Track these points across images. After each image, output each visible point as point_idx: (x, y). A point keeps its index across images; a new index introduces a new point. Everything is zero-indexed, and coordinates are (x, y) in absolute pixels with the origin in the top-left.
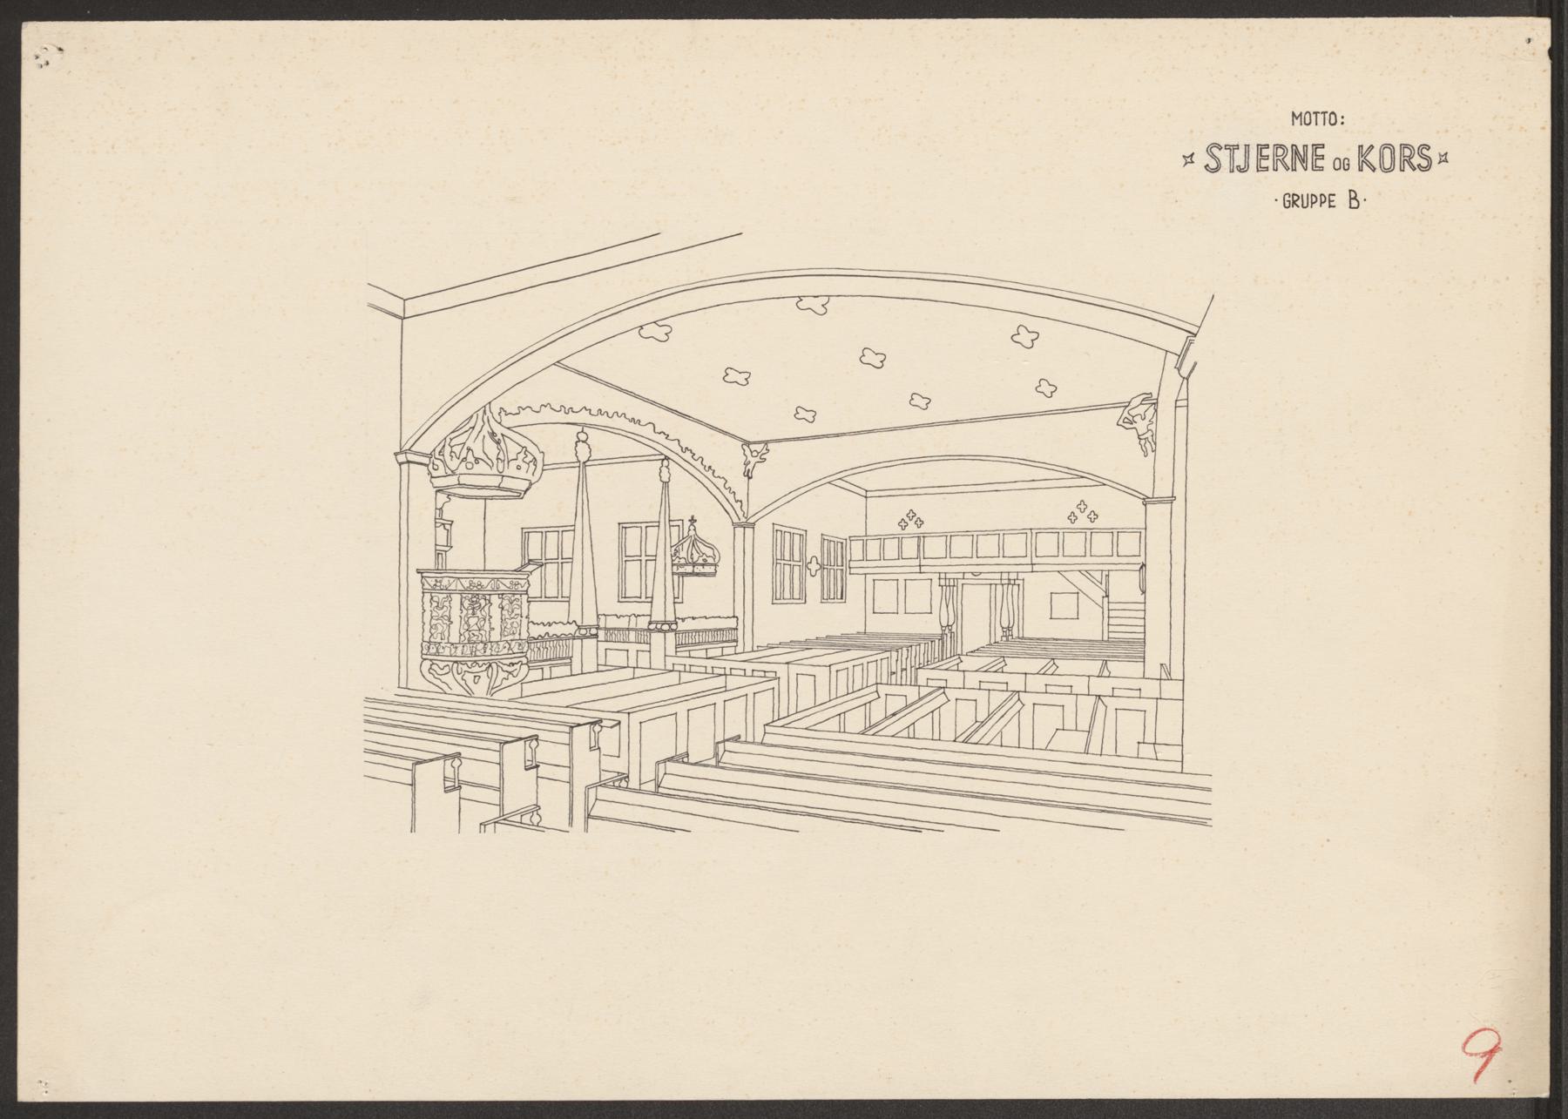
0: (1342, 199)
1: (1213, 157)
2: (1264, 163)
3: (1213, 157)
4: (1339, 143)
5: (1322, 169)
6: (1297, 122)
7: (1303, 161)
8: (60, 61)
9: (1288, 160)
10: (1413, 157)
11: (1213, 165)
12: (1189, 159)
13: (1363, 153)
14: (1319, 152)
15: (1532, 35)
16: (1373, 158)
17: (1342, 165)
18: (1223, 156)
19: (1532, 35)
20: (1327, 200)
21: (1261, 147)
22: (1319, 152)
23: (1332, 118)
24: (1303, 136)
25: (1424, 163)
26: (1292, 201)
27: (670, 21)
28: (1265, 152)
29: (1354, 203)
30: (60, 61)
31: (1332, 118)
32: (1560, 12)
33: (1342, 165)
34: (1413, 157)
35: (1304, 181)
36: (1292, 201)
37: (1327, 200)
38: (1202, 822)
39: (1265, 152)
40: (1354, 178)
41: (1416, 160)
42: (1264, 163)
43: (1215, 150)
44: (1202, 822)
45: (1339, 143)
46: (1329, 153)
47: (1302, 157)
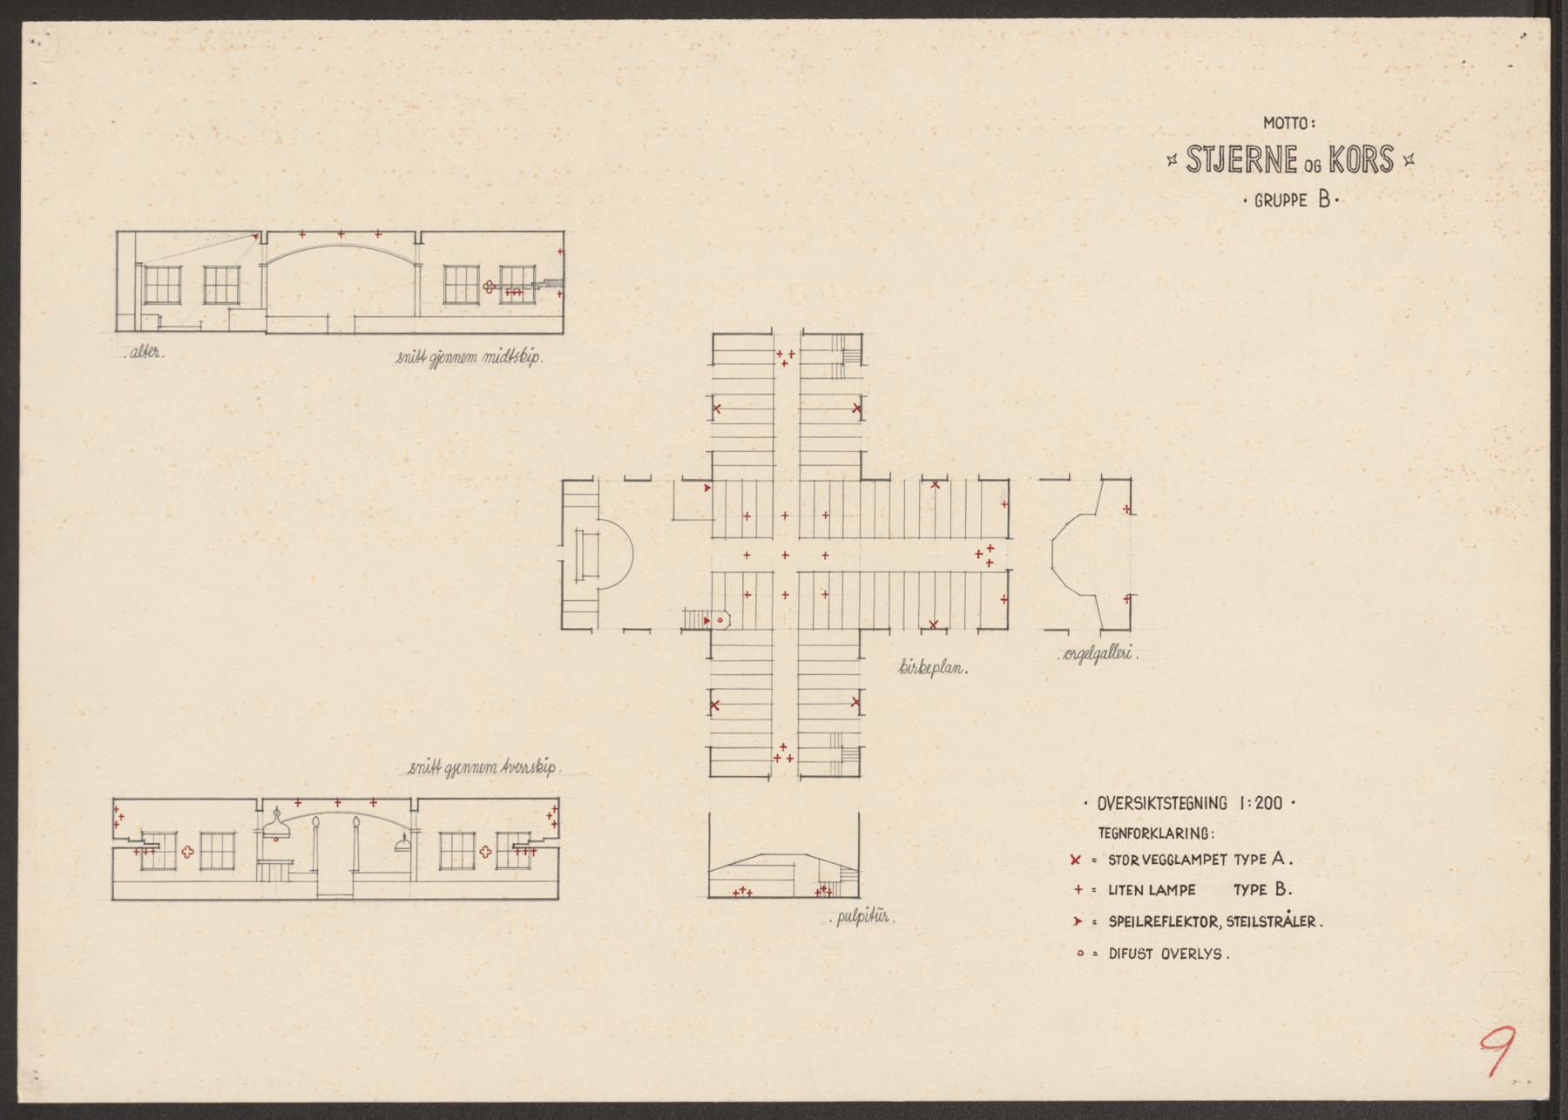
0: (1312, 199)
1: (1195, 158)
2: (1237, 165)
3: (1195, 158)
4: (1311, 145)
5: (1295, 170)
6: (1269, 126)
7: (1269, 157)
8: (59, 59)
9: (1262, 162)
10: (1368, 159)
11: (1194, 165)
12: (1172, 160)
13: (1334, 153)
14: (1293, 153)
15: (1532, 37)
16: (1342, 159)
17: (1314, 166)
18: (1202, 155)
19: (1532, 37)
20: (1297, 199)
21: (1233, 148)
22: (1293, 153)
23: (1301, 122)
24: (1273, 138)
25: (1195, 152)
26: (1266, 200)
27: (735, 21)
28: (1237, 153)
29: (1325, 202)
30: (59, 59)
31: (1301, 122)
32: (1559, 13)
33: (1314, 166)
34: (1368, 159)
35: (1278, 183)
36: (1266, 200)
37: (1297, 199)
38: (1106, 803)
39: (1237, 153)
40: (1327, 179)
41: (1380, 161)
42: (1237, 165)
43: (1195, 152)
44: (1106, 803)
45: (1311, 145)
46: (1301, 156)
47: (1281, 160)
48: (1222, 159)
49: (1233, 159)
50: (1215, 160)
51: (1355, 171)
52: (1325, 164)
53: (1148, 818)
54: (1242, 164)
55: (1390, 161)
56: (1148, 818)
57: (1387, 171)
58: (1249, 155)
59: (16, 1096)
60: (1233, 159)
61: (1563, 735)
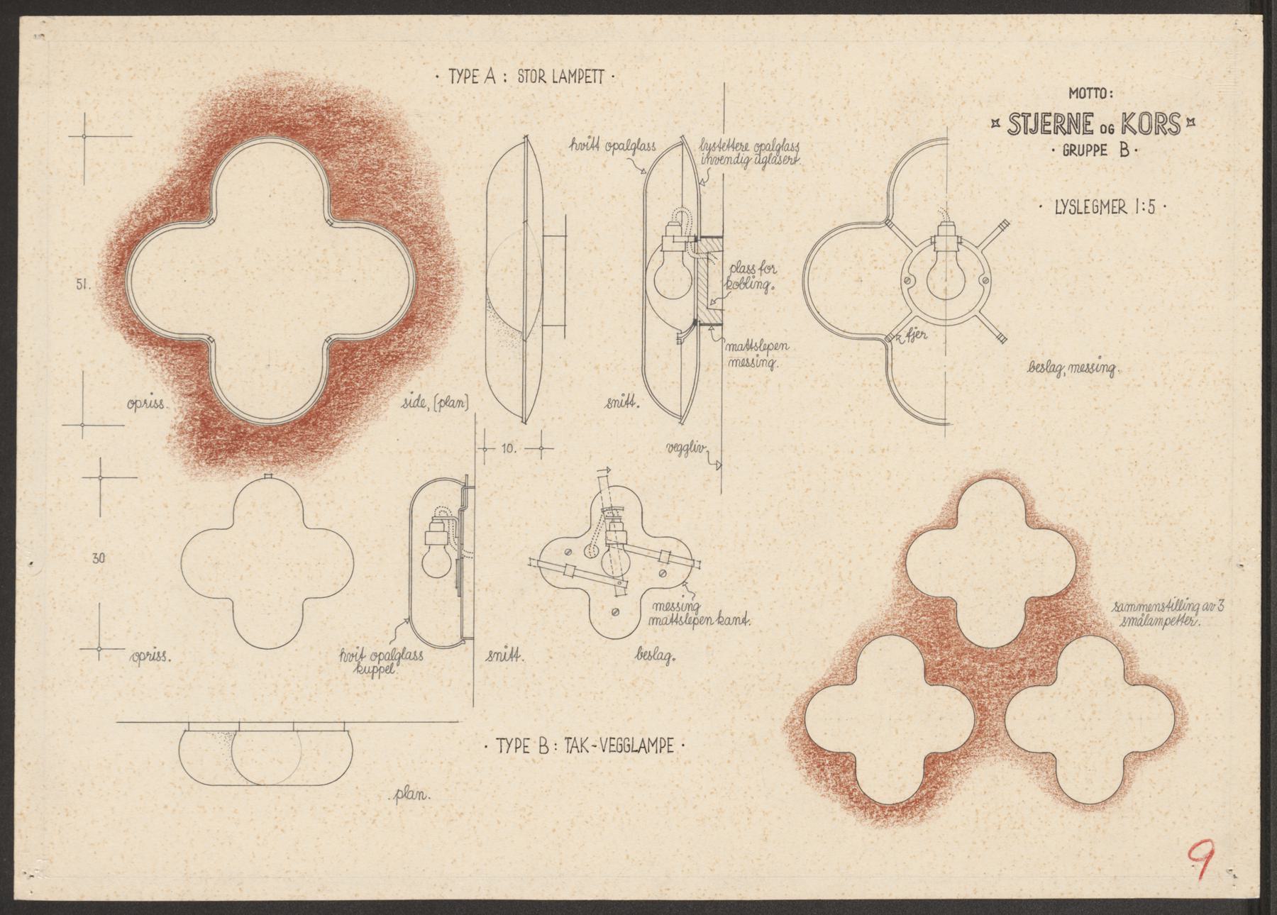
1: (1017, 124)
2: (1047, 128)
3: (1017, 124)
4: (1105, 112)
5: (1092, 132)
10: (1163, 124)
11: (1014, 128)
13: (1126, 118)
14: (1089, 119)
15: (1248, 30)
16: (1134, 123)
19: (1248, 30)
22: (1089, 119)
23: (1102, 93)
25: (1174, 129)
26: (1070, 150)
28: (1047, 119)
29: (1125, 152)
31: (1102, 93)
34: (1163, 124)
35: (1076, 139)
37: (1100, 149)
39: (1047, 119)
42: (1047, 128)
45: (1105, 112)
48: (1036, 124)
49: (1042, 123)
50: (1031, 125)
51: (1146, 133)
52: (1118, 128)
53: (534, 268)
54: (1051, 128)
55: (1178, 125)
56: (534, 268)
57: (1176, 133)
58: (1056, 121)
59: (12, 894)
60: (1042, 123)
61: (1273, 629)
